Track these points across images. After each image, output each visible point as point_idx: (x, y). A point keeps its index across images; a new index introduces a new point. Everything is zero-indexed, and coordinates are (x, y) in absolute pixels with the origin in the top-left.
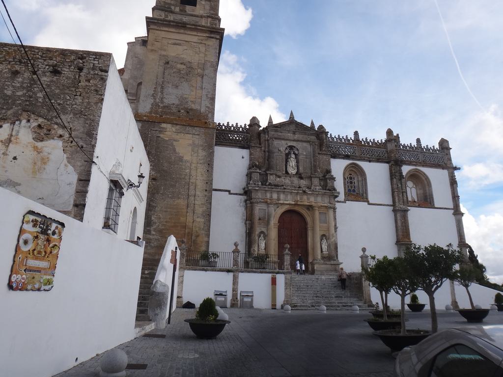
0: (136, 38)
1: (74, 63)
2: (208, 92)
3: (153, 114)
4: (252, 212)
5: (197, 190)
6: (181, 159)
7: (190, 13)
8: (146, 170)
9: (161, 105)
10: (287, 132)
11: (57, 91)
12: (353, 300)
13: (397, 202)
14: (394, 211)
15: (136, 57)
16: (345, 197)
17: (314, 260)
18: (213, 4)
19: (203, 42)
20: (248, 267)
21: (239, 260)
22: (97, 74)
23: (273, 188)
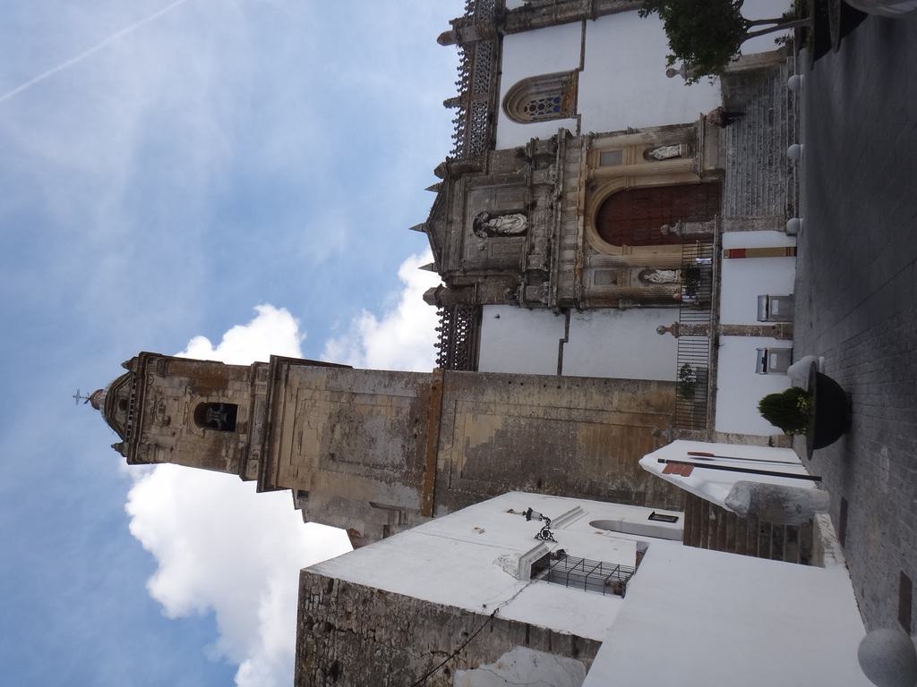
0: (296, 509)
1: (319, 638)
2: (380, 383)
3: (422, 483)
4: (599, 298)
6: (501, 434)
7: (248, 416)
8: (519, 499)
9: (406, 468)
10: (449, 235)
11: (368, 672)
12: (777, 87)
13: (576, 13)
14: (594, 16)
15: (327, 509)
16: (569, 117)
17: (695, 172)
18: (231, 376)
19: (295, 393)
20: (709, 304)
21: (694, 324)
22: (337, 598)
23: (554, 260)
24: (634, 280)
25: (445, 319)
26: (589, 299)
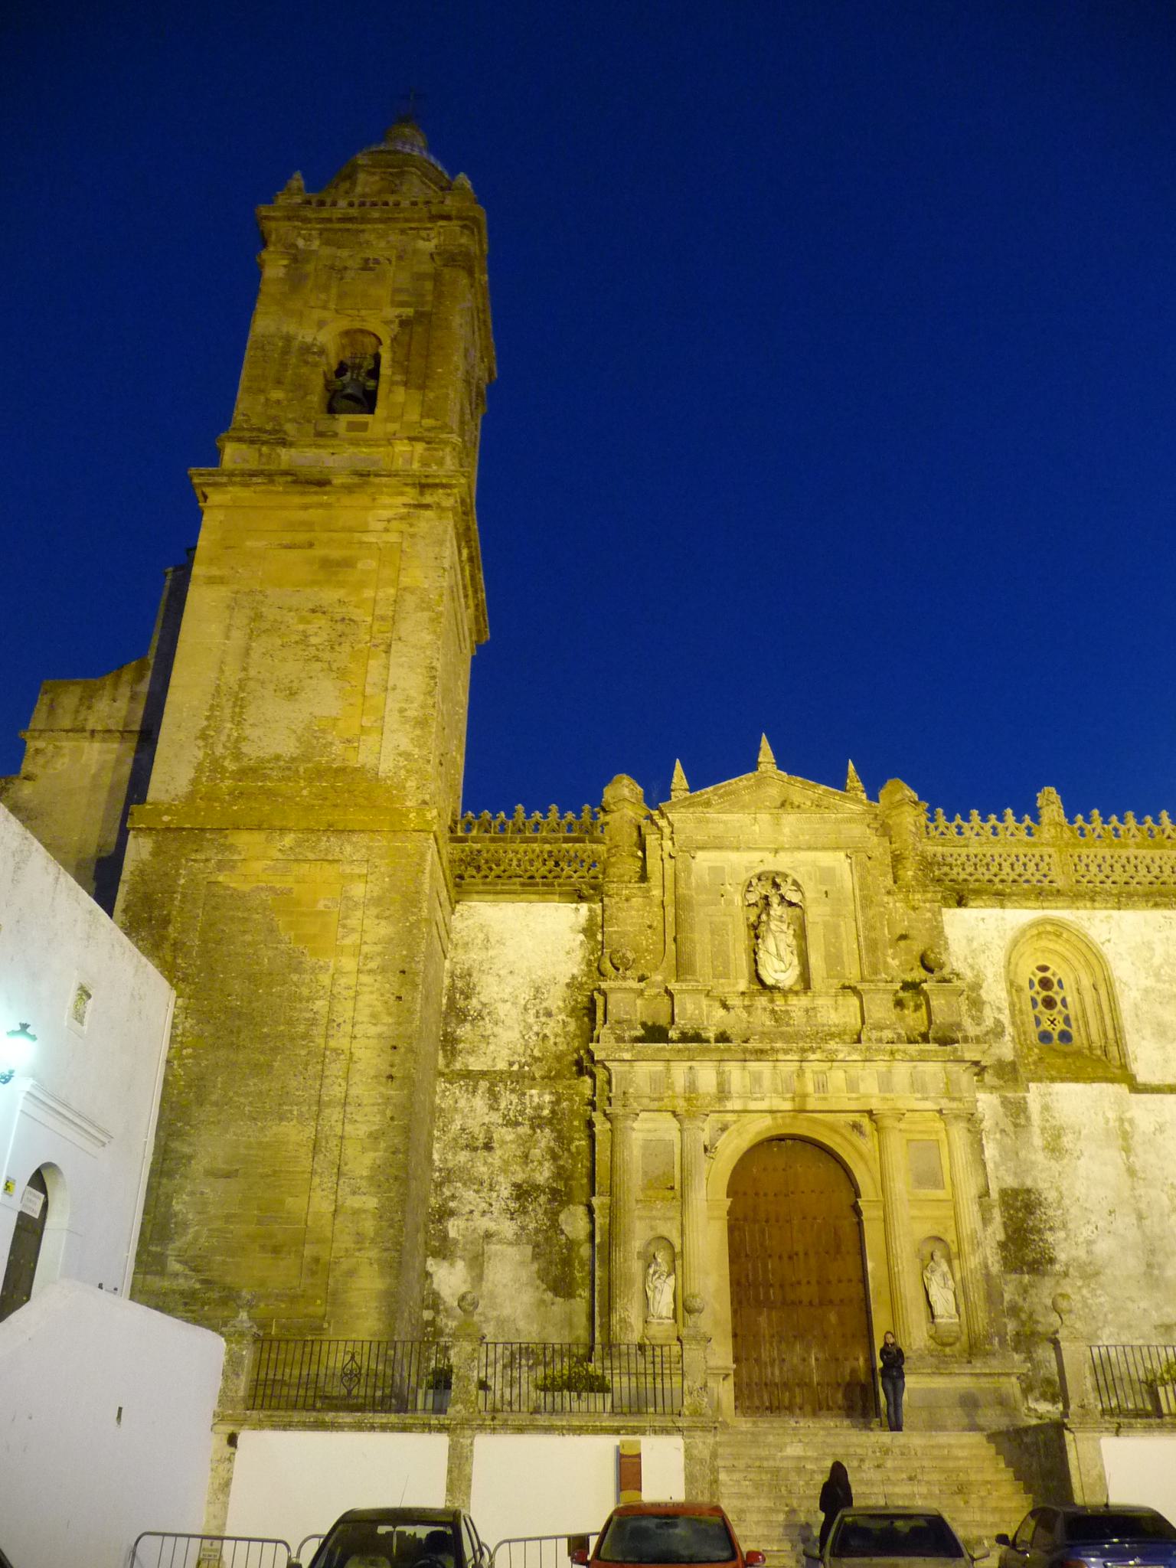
5: (355, 1078)
24: (652, 1228)
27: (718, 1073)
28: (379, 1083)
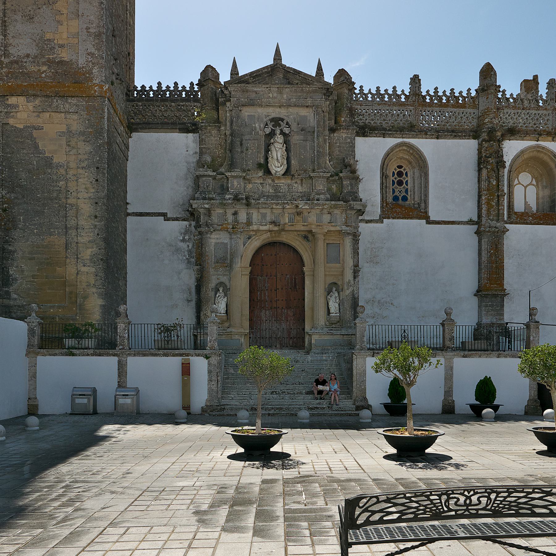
2: (91, 22)
6: (48, 163)
9: (6, 61)
25: (187, 92)
26: (201, 239)
27: (247, 214)
28: (91, 219)
